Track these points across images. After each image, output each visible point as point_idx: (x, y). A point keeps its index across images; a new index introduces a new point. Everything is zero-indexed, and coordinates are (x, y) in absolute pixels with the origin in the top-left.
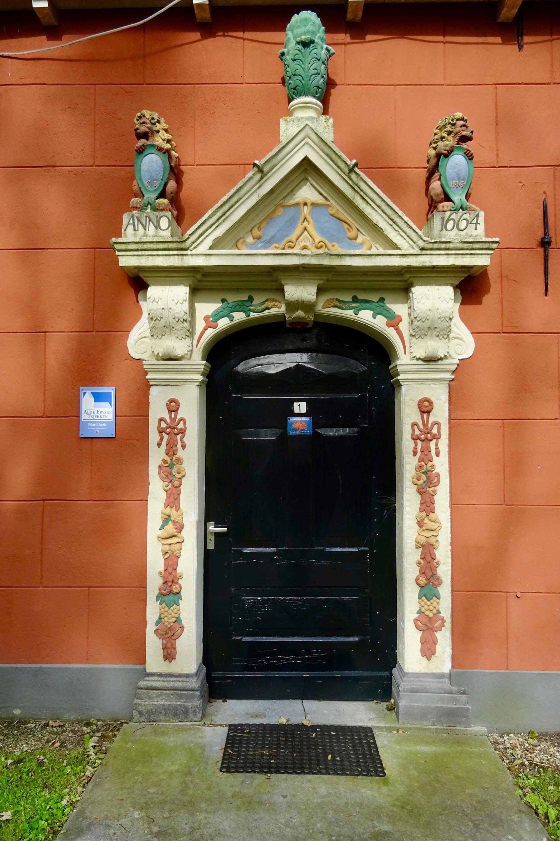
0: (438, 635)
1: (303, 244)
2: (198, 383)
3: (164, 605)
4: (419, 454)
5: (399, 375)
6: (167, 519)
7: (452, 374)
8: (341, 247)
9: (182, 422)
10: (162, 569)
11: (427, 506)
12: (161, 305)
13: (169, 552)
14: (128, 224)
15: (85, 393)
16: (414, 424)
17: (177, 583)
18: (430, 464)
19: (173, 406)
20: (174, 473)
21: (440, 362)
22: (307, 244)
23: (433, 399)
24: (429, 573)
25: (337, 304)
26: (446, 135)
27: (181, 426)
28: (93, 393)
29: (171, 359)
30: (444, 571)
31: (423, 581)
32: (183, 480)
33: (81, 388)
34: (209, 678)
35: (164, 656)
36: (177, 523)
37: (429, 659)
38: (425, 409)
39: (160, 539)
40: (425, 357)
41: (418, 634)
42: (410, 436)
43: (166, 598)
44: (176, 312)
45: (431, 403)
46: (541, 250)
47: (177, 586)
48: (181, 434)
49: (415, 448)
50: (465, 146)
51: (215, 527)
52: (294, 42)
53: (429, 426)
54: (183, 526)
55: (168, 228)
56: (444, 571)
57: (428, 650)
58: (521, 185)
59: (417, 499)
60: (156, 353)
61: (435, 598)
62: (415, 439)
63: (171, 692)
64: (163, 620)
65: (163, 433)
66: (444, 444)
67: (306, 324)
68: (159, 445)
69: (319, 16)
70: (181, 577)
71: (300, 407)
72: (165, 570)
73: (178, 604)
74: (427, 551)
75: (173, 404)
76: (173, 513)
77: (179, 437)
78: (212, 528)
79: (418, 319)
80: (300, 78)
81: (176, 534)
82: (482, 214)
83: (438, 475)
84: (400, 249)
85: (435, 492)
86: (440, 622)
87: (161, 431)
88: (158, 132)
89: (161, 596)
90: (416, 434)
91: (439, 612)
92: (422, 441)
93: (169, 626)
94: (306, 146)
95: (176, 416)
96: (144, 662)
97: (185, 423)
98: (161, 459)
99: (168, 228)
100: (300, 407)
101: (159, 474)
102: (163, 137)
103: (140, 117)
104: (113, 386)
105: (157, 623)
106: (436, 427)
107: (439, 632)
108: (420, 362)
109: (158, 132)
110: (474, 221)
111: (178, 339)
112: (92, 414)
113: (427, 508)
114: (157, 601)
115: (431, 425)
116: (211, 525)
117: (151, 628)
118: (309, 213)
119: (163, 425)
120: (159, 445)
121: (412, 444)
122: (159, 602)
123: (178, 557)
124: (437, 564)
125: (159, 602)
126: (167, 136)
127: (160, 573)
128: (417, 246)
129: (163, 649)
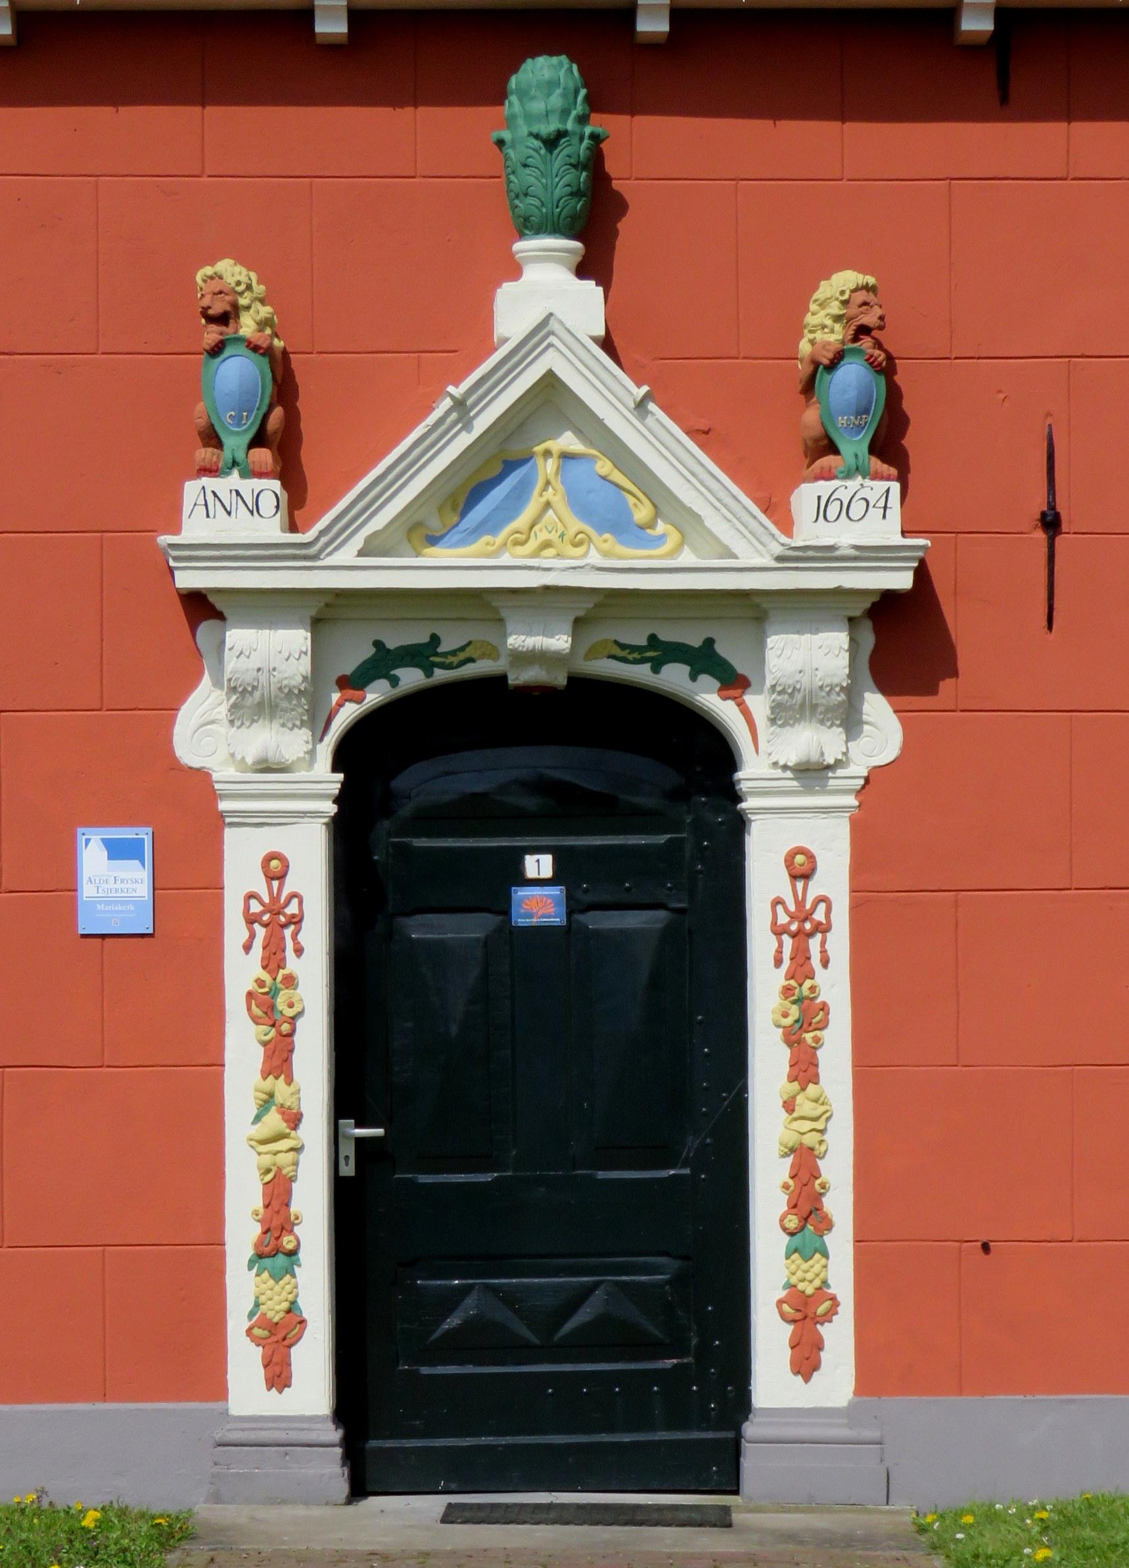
0: (824, 1330)
1: (543, 536)
2: (326, 820)
3: (266, 1275)
6: (267, 1102)
8: (621, 542)
9: (295, 901)
10: (259, 1204)
11: (804, 1069)
12: (253, 664)
15: (88, 841)
17: (291, 1232)
18: (808, 983)
19: (275, 868)
24: (805, 1208)
25: (618, 652)
26: (829, 322)
27: (293, 909)
28: (107, 843)
30: (840, 1203)
31: (793, 1222)
32: (300, 1023)
33: (80, 830)
37: (807, 1378)
38: (800, 870)
39: (253, 1143)
40: (798, 764)
41: (787, 1331)
43: (267, 1262)
44: (286, 675)
45: (811, 857)
46: (1040, 536)
47: (291, 1238)
48: (293, 927)
49: (779, 952)
53: (808, 906)
54: (301, 1115)
56: (840, 1203)
57: (806, 1360)
58: (1002, 396)
59: (784, 1054)
60: (239, 757)
61: (817, 1256)
62: (778, 931)
65: (256, 926)
66: (839, 942)
68: (247, 948)
71: (539, 865)
72: (266, 1206)
73: (294, 1276)
74: (805, 1164)
76: (280, 1086)
77: (288, 932)
79: (779, 688)
80: (537, 203)
82: (895, 487)
84: (735, 557)
86: (828, 1304)
87: (251, 920)
90: (252, 911)
92: (794, 936)
94: (551, 350)
97: (301, 903)
98: (255, 977)
100: (539, 865)
101: (249, 1009)
104: (146, 824)
106: (822, 907)
108: (789, 774)
111: (285, 729)
112: (105, 886)
114: (250, 1269)
116: (346, 1126)
118: (557, 473)
119: (255, 907)
120: (247, 948)
122: (255, 1270)
123: (292, 1180)
124: (823, 1188)
125: (255, 1270)
126: (265, 311)
128: (768, 552)
129: (265, 1366)
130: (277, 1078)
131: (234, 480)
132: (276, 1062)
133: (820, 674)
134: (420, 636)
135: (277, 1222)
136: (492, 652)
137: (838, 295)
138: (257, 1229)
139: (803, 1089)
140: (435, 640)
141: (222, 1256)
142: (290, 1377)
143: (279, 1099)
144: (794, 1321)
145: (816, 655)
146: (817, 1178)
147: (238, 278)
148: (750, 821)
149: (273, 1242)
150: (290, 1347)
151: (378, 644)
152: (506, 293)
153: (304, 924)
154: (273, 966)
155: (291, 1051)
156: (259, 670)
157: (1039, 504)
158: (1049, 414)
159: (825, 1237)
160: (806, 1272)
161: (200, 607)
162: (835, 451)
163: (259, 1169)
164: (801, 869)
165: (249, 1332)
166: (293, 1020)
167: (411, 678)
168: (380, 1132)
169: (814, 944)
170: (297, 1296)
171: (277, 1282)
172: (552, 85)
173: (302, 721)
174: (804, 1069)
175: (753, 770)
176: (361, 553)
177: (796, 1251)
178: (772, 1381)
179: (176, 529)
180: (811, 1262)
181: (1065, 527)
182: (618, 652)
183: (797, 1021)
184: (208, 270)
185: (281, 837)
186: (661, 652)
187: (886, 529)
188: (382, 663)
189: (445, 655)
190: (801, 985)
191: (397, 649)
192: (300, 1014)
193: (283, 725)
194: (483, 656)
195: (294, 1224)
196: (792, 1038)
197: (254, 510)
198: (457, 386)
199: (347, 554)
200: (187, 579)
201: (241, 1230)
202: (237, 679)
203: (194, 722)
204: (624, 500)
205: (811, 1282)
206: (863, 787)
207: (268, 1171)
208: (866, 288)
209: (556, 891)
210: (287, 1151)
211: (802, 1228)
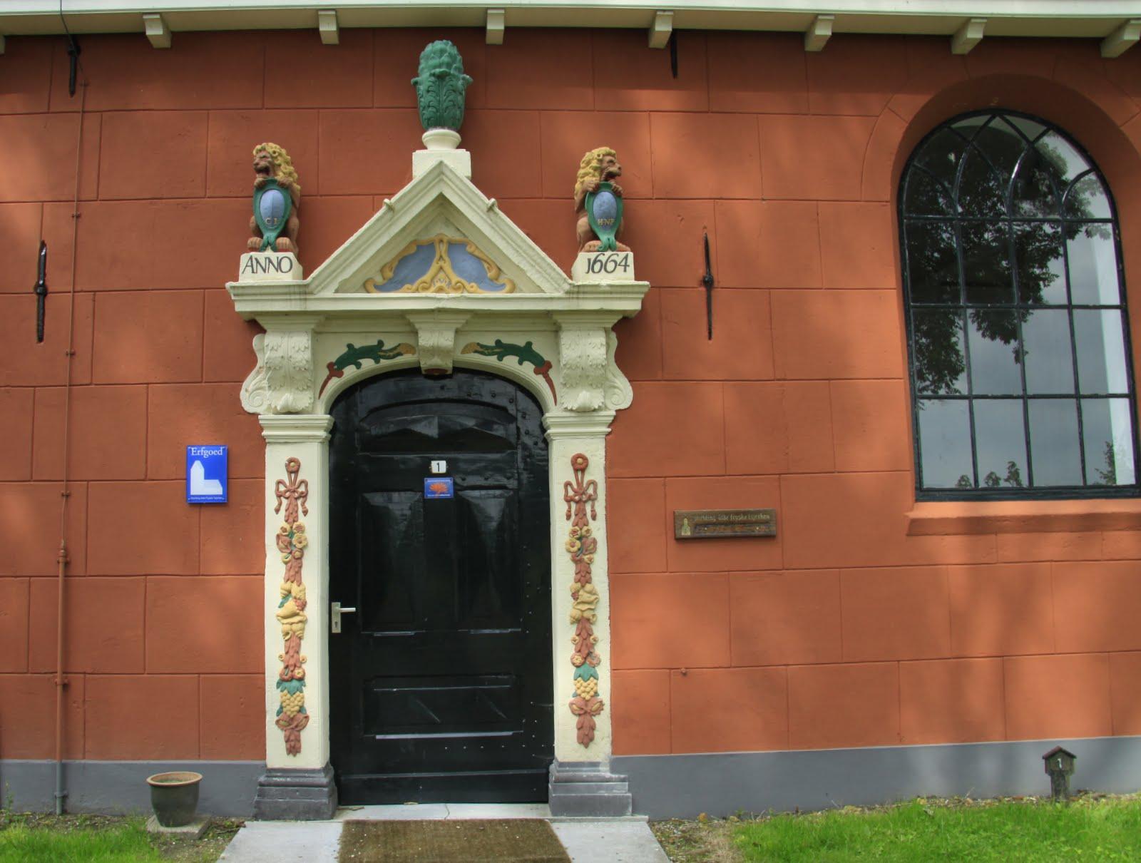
0: (597, 719)
1: (438, 284)
2: (321, 440)
3: (286, 692)
4: (573, 517)
5: (549, 429)
6: (287, 595)
7: (609, 426)
10: (283, 652)
11: (584, 576)
12: (280, 353)
13: (291, 632)
14: (246, 266)
16: (568, 484)
17: (300, 667)
19: (293, 467)
20: (294, 542)
21: (595, 414)
22: (443, 284)
23: (588, 455)
25: (479, 349)
26: (592, 171)
29: (290, 413)
31: (579, 660)
32: (306, 552)
34: (337, 779)
35: (287, 749)
36: (299, 599)
37: (586, 746)
38: (578, 467)
39: (279, 618)
42: (563, 497)
43: (287, 684)
45: (585, 459)
46: (703, 289)
47: (300, 670)
49: (569, 511)
50: (612, 182)
51: (342, 606)
52: (428, 74)
53: (584, 486)
54: (306, 602)
55: (290, 270)
57: (586, 737)
58: (680, 218)
59: (572, 568)
60: (273, 406)
61: (592, 678)
62: (568, 500)
63: (296, 788)
64: (284, 709)
65: (282, 498)
67: (445, 371)
68: (277, 511)
69: (454, 43)
70: (304, 661)
71: (439, 466)
73: (301, 692)
75: (292, 464)
76: (295, 589)
77: (299, 502)
78: (337, 607)
79: (568, 366)
81: (298, 611)
82: (631, 255)
83: (595, 542)
84: (543, 291)
85: (591, 560)
88: (280, 165)
89: (282, 681)
91: (596, 694)
92: (577, 502)
93: (292, 716)
95: (296, 478)
96: (263, 756)
97: (306, 486)
99: (290, 270)
101: (278, 544)
102: (285, 171)
103: (260, 151)
105: (279, 713)
107: (597, 716)
108: (573, 414)
109: (280, 165)
110: (623, 263)
113: (582, 578)
114: (278, 687)
115: (587, 484)
116: (337, 605)
117: (271, 718)
119: (282, 488)
120: (277, 511)
121: (565, 507)
123: (300, 638)
127: (281, 657)
130: (292, 582)
131: (269, 253)
132: (292, 573)
133: (591, 358)
134: (372, 341)
135: (292, 662)
136: (412, 349)
137: (596, 156)
138: (282, 666)
139: (583, 587)
140: (381, 343)
141: (264, 680)
142: (300, 748)
143: (293, 594)
144: (580, 715)
145: (591, 348)
146: (590, 635)
147: (274, 149)
148: (552, 440)
149: (290, 673)
150: (299, 731)
151: (350, 346)
152: (417, 156)
153: (308, 497)
154: (291, 520)
155: (300, 567)
156: (282, 357)
157: (701, 272)
158: (705, 228)
159: (596, 668)
160: (586, 687)
161: (254, 325)
162: (596, 238)
163: (282, 632)
164: (580, 465)
165: (277, 722)
166: (301, 550)
167: (368, 364)
168: (353, 609)
169: (588, 508)
170: (303, 702)
171: (292, 696)
172: (442, 52)
173: (308, 387)
174: (584, 576)
175: (553, 414)
176: (337, 291)
177: (580, 676)
178: (566, 744)
179: (236, 279)
180: (589, 682)
181: (716, 284)
182: (479, 349)
183: (579, 549)
184: (259, 147)
185: (297, 459)
186: (503, 350)
187: (627, 277)
188: (353, 356)
189: (385, 351)
190: (581, 529)
191: (360, 348)
192: (305, 547)
193: (298, 389)
194: (407, 352)
195: (301, 663)
196: (577, 560)
197: (279, 268)
198: (390, 199)
199: (329, 293)
200: (243, 307)
201: (273, 667)
202: (271, 363)
203: (251, 388)
204: (487, 269)
205: (588, 692)
206: (613, 421)
207: (287, 634)
208: (609, 154)
209: (448, 481)
210: (297, 623)
211: (583, 664)
